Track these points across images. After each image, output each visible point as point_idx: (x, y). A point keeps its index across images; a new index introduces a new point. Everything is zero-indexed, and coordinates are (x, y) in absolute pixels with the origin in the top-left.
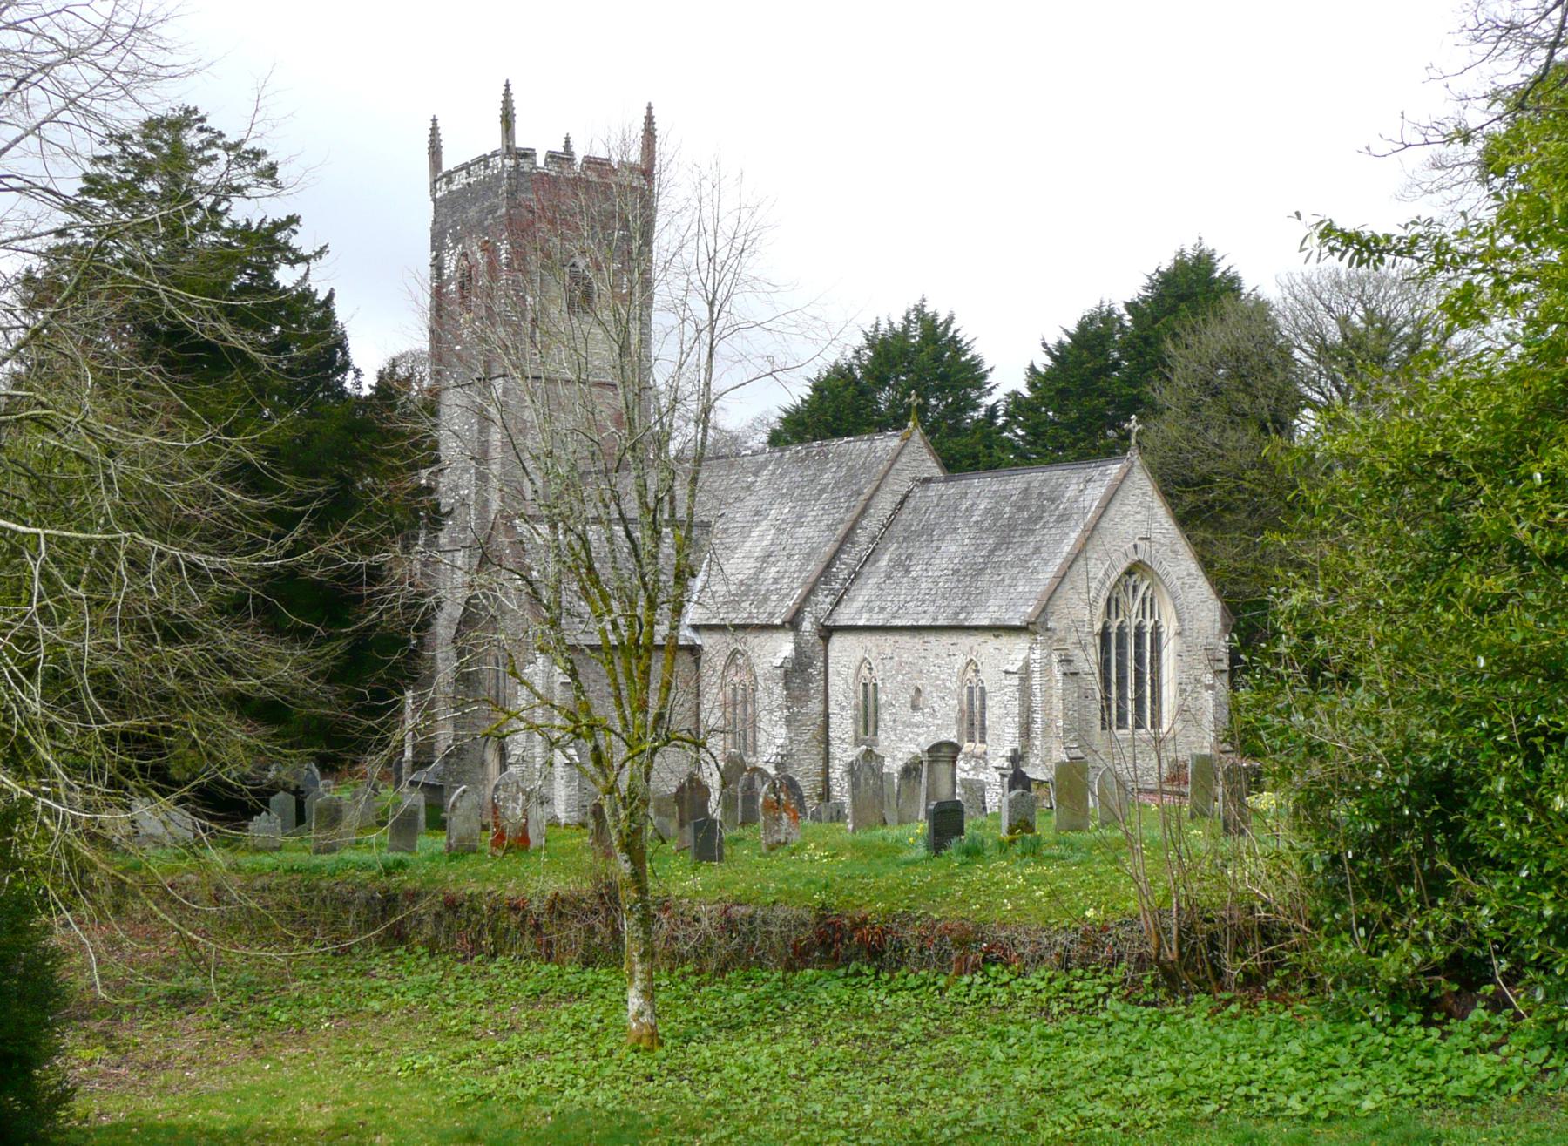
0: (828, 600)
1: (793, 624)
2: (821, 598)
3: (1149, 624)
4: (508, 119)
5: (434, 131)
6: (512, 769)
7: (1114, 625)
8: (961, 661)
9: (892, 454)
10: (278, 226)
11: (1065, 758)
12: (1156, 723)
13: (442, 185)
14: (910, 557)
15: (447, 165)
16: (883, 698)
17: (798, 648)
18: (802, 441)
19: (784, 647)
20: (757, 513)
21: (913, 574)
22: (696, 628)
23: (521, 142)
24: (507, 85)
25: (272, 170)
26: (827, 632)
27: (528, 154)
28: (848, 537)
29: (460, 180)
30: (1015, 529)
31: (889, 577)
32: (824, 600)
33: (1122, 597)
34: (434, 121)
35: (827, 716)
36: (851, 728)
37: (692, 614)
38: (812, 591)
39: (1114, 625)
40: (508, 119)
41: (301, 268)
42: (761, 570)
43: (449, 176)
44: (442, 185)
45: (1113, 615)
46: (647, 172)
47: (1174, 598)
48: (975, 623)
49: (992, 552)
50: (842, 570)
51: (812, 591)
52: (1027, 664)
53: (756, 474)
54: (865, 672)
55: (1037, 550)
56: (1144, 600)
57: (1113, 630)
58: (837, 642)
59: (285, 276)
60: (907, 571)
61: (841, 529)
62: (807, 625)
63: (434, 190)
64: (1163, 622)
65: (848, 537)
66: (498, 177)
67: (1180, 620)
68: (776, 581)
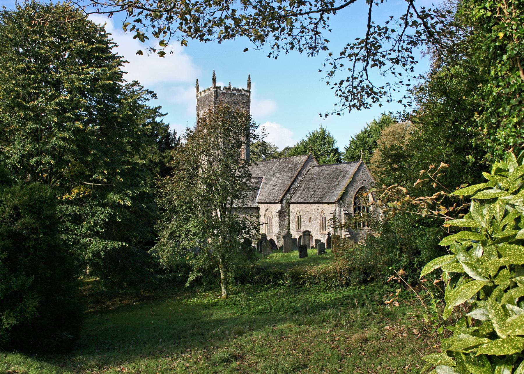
1: (281, 202)
4: (214, 80)
6: (505, 231)
8: (320, 211)
9: (305, 160)
10: (156, 108)
13: (199, 95)
15: (201, 89)
16: (302, 220)
17: (282, 207)
18: (136, 163)
19: (278, 207)
20: (274, 175)
22: (259, 203)
23: (217, 84)
25: (155, 94)
26: (289, 204)
28: (295, 181)
29: (203, 94)
32: (288, 196)
35: (289, 224)
36: (295, 227)
37: (257, 199)
38: (285, 194)
40: (214, 80)
41: (162, 117)
42: (274, 189)
43: (201, 93)
44: (199, 95)
50: (292, 189)
51: (285, 194)
52: (335, 211)
54: (322, 214)
58: (291, 205)
59: (158, 119)
61: (293, 179)
62: (284, 202)
63: (197, 96)
65: (295, 181)
66: (212, 93)
68: (277, 191)
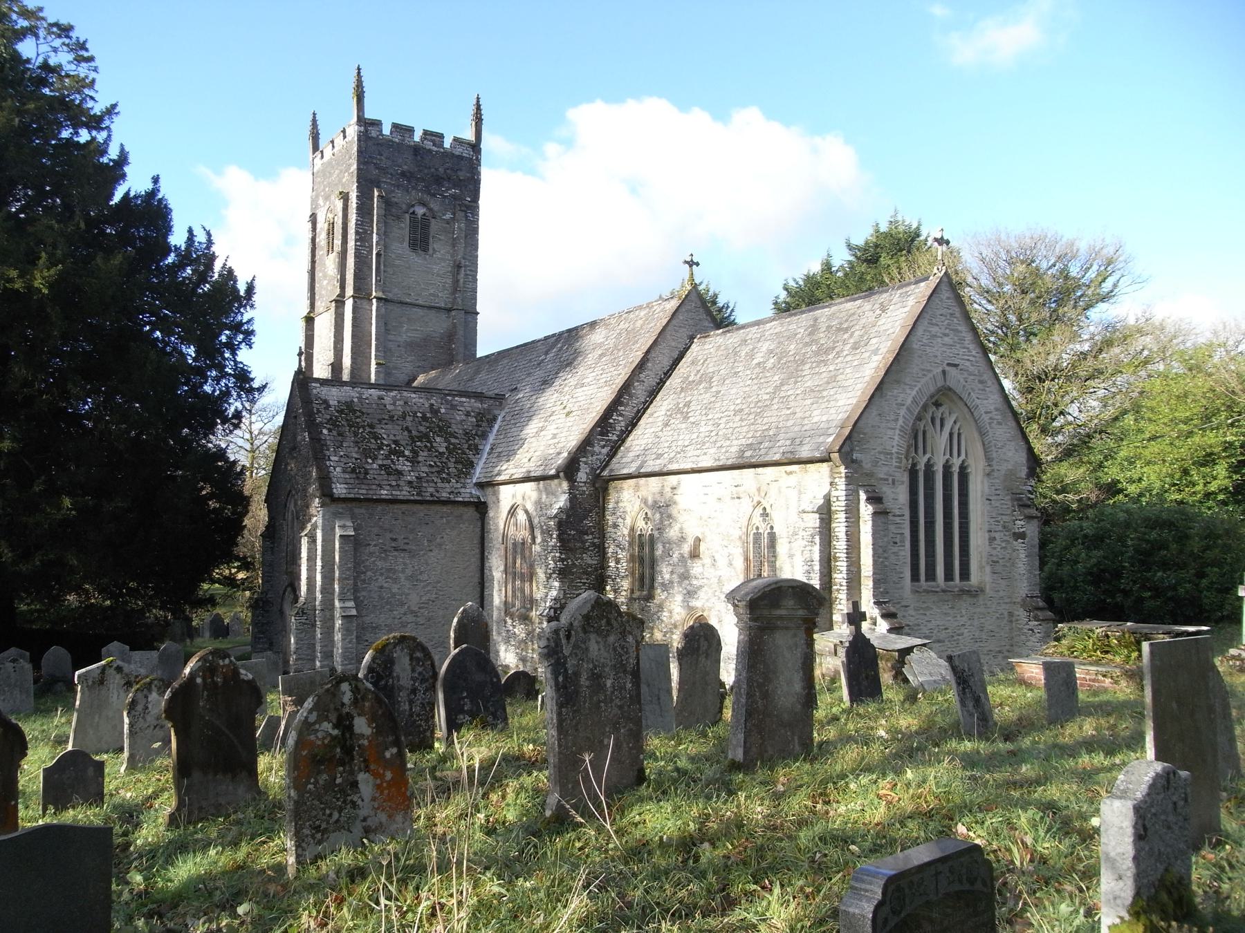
0: (605, 451)
2: (597, 449)
3: (956, 463)
5: (314, 122)
7: (922, 461)
11: (226, 621)
12: (965, 575)
14: (688, 404)
17: (573, 499)
21: (691, 419)
23: (369, 115)
24: (359, 69)
27: (377, 124)
30: (803, 363)
31: (667, 425)
33: (930, 428)
34: (314, 114)
39: (922, 461)
45: (921, 450)
46: (476, 147)
47: (982, 434)
48: (767, 459)
49: (778, 388)
53: (546, 353)
55: (833, 379)
56: (951, 435)
57: (921, 467)
60: (686, 418)
62: (582, 476)
64: (971, 462)
67: (989, 459)
